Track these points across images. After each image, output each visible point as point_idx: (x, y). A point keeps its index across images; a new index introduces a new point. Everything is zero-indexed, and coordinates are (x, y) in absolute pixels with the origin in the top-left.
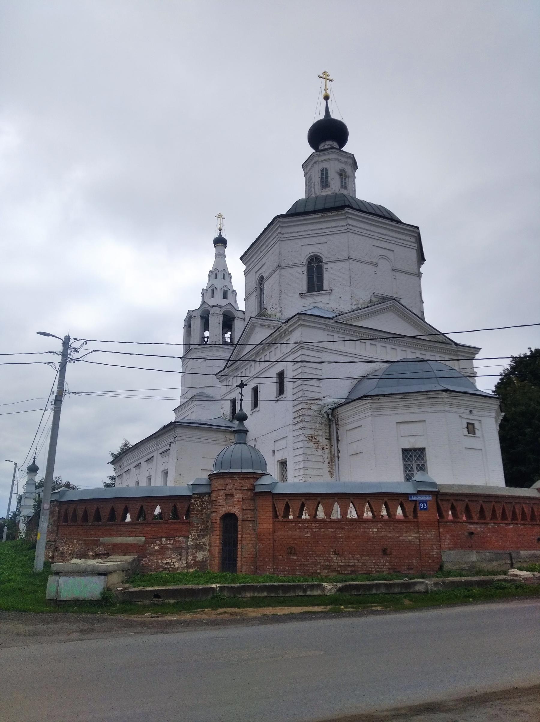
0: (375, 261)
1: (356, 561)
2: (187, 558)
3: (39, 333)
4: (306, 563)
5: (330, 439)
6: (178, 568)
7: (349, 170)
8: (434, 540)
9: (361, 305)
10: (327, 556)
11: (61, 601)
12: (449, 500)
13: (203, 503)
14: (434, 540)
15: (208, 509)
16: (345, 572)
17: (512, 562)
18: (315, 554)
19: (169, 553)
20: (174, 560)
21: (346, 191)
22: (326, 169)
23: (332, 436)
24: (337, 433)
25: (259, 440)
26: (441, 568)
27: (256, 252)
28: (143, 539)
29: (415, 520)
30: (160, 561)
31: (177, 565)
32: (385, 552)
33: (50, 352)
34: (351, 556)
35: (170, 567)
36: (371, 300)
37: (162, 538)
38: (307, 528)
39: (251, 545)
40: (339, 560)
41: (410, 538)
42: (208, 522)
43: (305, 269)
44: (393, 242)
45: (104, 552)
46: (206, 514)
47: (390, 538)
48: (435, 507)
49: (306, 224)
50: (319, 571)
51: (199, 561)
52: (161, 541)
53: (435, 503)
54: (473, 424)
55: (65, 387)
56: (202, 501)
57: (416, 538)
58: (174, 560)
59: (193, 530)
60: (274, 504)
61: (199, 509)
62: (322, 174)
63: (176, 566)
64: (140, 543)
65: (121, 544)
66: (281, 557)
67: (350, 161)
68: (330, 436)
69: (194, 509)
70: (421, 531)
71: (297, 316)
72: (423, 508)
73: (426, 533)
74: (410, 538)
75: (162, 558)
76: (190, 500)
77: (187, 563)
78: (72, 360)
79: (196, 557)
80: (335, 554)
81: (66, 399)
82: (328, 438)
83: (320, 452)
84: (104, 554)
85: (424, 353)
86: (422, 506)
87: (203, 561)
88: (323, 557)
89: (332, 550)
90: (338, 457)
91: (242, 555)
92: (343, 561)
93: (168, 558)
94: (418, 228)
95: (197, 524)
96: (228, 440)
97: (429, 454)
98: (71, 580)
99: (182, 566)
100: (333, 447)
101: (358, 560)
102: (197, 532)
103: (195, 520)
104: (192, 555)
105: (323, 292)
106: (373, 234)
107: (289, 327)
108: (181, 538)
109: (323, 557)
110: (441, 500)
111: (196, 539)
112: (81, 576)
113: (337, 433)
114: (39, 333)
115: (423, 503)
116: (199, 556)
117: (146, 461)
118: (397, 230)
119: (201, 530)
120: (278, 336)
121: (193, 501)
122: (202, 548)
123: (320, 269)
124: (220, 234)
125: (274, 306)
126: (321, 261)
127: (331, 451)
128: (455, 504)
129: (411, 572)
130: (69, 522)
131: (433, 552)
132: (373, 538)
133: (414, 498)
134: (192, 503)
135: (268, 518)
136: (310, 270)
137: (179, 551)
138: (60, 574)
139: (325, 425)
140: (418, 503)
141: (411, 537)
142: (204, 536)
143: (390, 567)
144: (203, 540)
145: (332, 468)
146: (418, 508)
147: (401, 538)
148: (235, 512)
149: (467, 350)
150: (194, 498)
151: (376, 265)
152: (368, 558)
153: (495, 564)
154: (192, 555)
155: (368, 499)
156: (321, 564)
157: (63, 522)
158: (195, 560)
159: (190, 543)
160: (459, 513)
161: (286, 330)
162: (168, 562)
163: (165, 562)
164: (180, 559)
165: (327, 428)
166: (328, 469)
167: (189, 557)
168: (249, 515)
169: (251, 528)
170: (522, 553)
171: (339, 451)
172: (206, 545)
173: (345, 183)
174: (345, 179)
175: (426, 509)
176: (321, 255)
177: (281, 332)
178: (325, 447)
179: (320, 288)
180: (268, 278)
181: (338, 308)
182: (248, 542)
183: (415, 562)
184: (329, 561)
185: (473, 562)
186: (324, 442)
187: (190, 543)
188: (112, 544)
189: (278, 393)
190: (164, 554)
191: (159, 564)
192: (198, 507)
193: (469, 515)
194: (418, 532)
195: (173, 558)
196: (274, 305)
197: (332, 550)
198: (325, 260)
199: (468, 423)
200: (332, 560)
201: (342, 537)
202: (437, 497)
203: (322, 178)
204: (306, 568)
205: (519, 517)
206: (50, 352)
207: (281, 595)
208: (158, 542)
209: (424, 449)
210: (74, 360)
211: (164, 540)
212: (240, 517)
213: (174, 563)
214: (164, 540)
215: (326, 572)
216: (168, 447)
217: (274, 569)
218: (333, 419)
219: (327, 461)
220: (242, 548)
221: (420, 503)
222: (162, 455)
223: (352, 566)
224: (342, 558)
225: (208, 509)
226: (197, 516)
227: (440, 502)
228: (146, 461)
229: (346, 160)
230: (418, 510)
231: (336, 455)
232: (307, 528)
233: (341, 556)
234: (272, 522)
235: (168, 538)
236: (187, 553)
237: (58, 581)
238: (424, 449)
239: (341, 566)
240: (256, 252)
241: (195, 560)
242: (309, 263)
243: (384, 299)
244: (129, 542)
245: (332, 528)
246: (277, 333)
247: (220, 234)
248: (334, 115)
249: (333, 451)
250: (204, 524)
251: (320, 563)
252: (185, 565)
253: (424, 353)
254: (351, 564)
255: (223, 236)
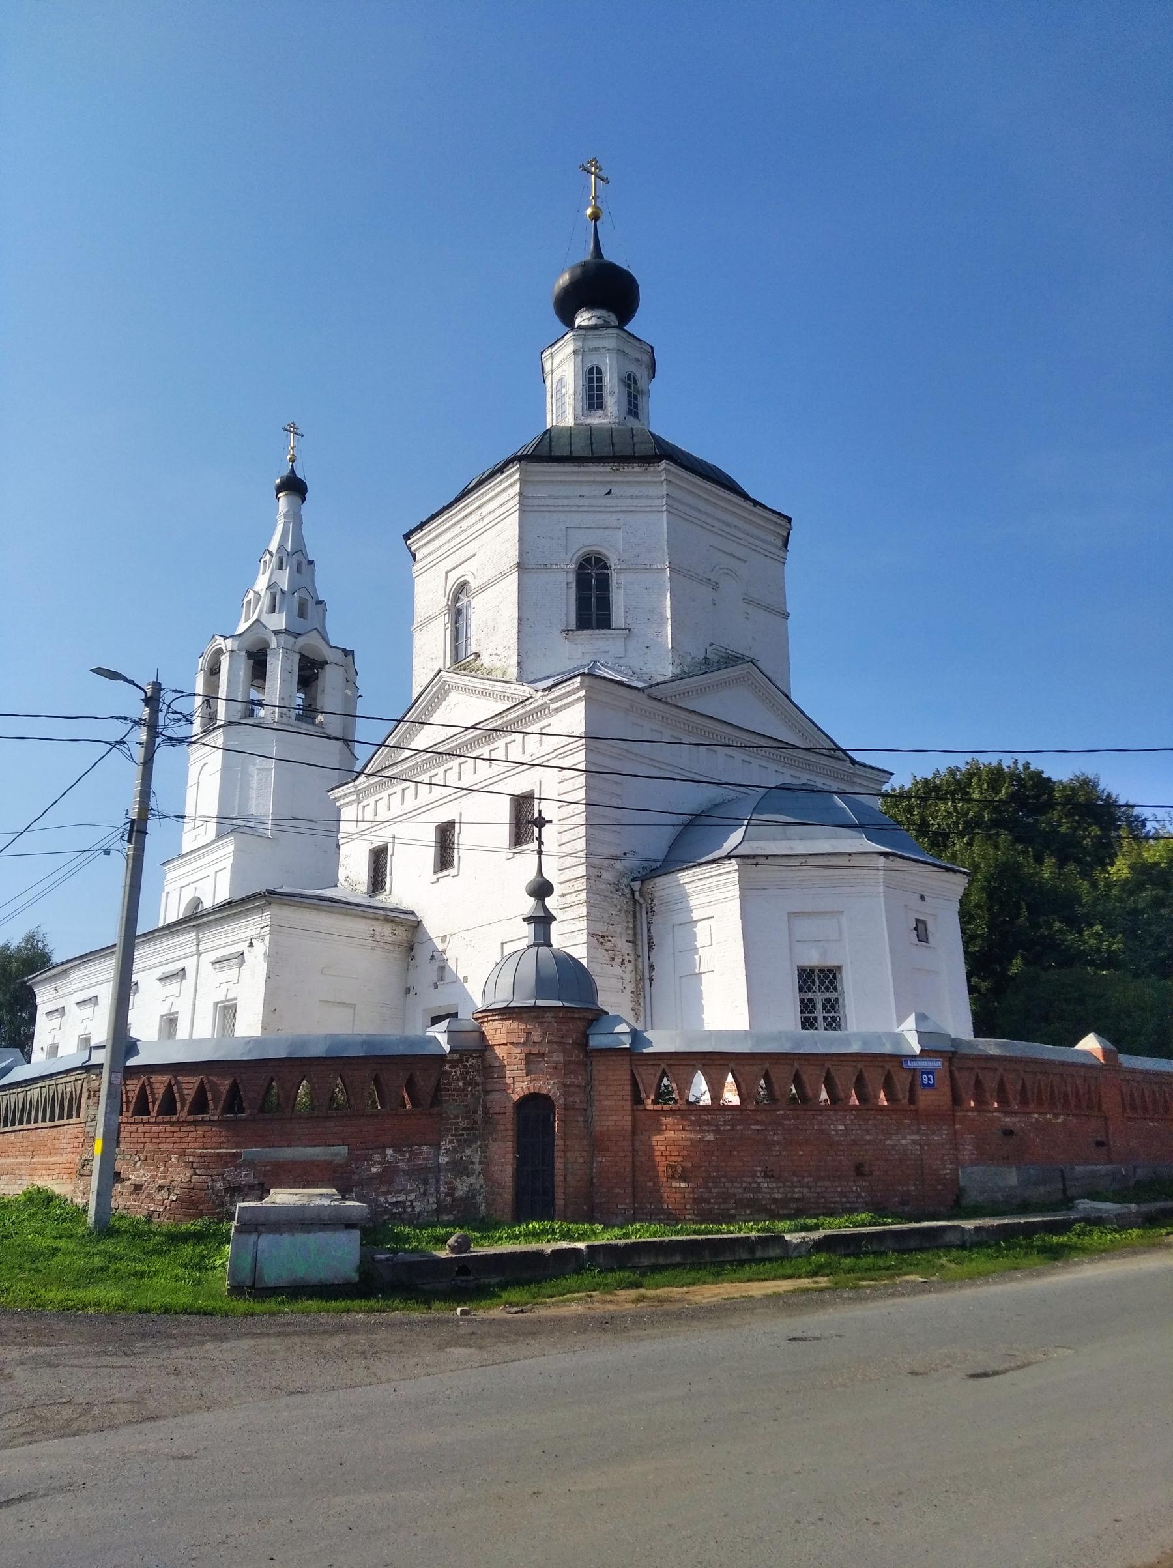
0: (713, 577)
1: (805, 1190)
2: (438, 1192)
3: (99, 671)
4: (706, 1196)
5: (633, 942)
6: (420, 1213)
7: (641, 374)
8: (947, 1147)
9: (689, 667)
10: (749, 1180)
11: (263, 1289)
12: (972, 1069)
13: (468, 1073)
14: (947, 1147)
15: (477, 1084)
16: (785, 1212)
17: (1064, 1185)
18: (725, 1176)
19: (400, 1181)
20: (412, 1196)
21: (636, 421)
22: (599, 371)
23: (639, 937)
24: (649, 930)
25: (455, 939)
26: (957, 1202)
27: (448, 529)
28: (344, 1150)
29: (912, 1107)
30: (382, 1199)
31: (418, 1207)
32: (859, 1171)
33: (119, 718)
34: (795, 1179)
35: (405, 1212)
36: (706, 658)
37: (385, 1147)
38: (708, 1123)
39: (581, 1160)
40: (772, 1188)
41: (903, 1142)
42: (475, 1112)
43: (572, 578)
44: (746, 543)
45: (252, 1180)
46: (472, 1095)
47: (869, 1142)
48: (948, 1083)
49: (576, 482)
50: (732, 1212)
51: (461, 1198)
52: (384, 1155)
53: (948, 1074)
54: (924, 923)
55: (153, 803)
56: (465, 1066)
57: (914, 1142)
58: (412, 1196)
59: (448, 1130)
60: (633, 1076)
61: (460, 1084)
62: (590, 380)
63: (417, 1210)
64: (338, 1160)
65: (294, 1163)
66: (650, 1184)
67: (646, 358)
68: (635, 935)
69: (449, 1084)
70: (924, 1128)
71: (579, 679)
72: (928, 1085)
73: (933, 1133)
74: (903, 1142)
75: (389, 1192)
76: (442, 1066)
77: (438, 1202)
78: (170, 739)
79: (454, 1189)
80: (766, 1176)
81: (152, 825)
82: (631, 939)
83: (617, 970)
84: (252, 1187)
85: (797, 774)
86: (925, 1078)
87: (467, 1198)
88: (741, 1183)
89: (759, 1169)
90: (651, 980)
91: (565, 1182)
92: (782, 1190)
93: (400, 1192)
94: (789, 520)
95: (456, 1117)
96: (378, 937)
97: (848, 980)
98: (286, 1239)
99: (429, 1208)
100: (640, 960)
101: (809, 1188)
102: (455, 1135)
103: (452, 1108)
104: (446, 1183)
105: (608, 631)
106: (709, 520)
107: (553, 700)
108: (425, 1148)
109: (741, 1183)
110: (959, 1069)
111: (455, 1150)
112: (309, 1232)
113: (649, 930)
114: (99, 671)
115: (927, 1074)
116: (460, 1187)
117: (160, 979)
118: (752, 518)
119: (463, 1129)
120: (520, 719)
121: (447, 1067)
122: (466, 1168)
123: (604, 583)
124: (292, 471)
125: (500, 650)
126: (606, 567)
127: (636, 966)
128: (981, 1077)
129: (906, 1209)
130: (153, 1114)
131: (945, 1169)
132: (839, 1143)
133: (912, 1064)
134: (446, 1072)
135: (622, 1103)
136: (582, 582)
137: (422, 1176)
138: (261, 1228)
139: (626, 911)
140: (918, 1073)
141: (907, 1140)
142: (469, 1143)
143: (868, 1199)
144: (468, 1152)
145: (638, 1003)
146: (918, 1083)
147: (888, 1142)
148: (550, 1091)
149: (870, 774)
150: (449, 1062)
151: (716, 586)
152: (827, 1183)
153: (1042, 1189)
154: (446, 1183)
155: (732, 1065)
156: (738, 1196)
157: (190, 1113)
158: (451, 1195)
159: (443, 1159)
160: (988, 1095)
161: (544, 707)
162: (399, 1199)
163: (394, 1200)
164: (425, 1194)
165: (631, 916)
166: (631, 1005)
167: (442, 1189)
168: (577, 1099)
169: (581, 1124)
170: (1079, 1169)
171: (652, 968)
172: (473, 1163)
173: (636, 406)
174: (636, 398)
175: (933, 1085)
176: (596, 548)
177: (528, 708)
178: (627, 958)
179: (604, 623)
180: (482, 589)
181: (644, 669)
182: (578, 1154)
183: (913, 1188)
184: (754, 1191)
185: (1011, 1188)
186: (624, 947)
187: (443, 1159)
188: (269, 1163)
189: (513, 840)
190: (391, 1182)
191: (380, 1206)
192: (458, 1080)
193: (1004, 1101)
194: (918, 1132)
195: (412, 1191)
196: (500, 648)
197: (759, 1169)
198: (613, 563)
199: (917, 921)
200: (759, 1189)
201: (779, 1143)
202: (951, 1064)
203: (591, 388)
204: (706, 1207)
205: (1073, 1102)
206: (119, 718)
207: (708, 1259)
208: (377, 1157)
209: (839, 968)
210: (174, 741)
211: (389, 1151)
212: (559, 1103)
213: (411, 1201)
214: (389, 1151)
215: (748, 1212)
216: (243, 947)
217: (634, 1209)
218: (641, 901)
219: (630, 987)
220: (565, 1169)
221: (923, 1073)
222: (217, 966)
223: (798, 1200)
224: (780, 1185)
225: (477, 1084)
226: (456, 1101)
227: (956, 1073)
228: (160, 979)
229: (638, 356)
230: (919, 1087)
231: (647, 975)
232: (708, 1123)
233: (778, 1179)
234: (629, 1112)
235: (397, 1149)
236: (438, 1181)
237: (256, 1244)
238: (839, 968)
239: (775, 1201)
240: (448, 529)
241: (451, 1195)
242: (581, 567)
243: (731, 660)
244: (315, 1158)
245: (757, 1123)
246: (520, 711)
247: (292, 471)
248: (611, 255)
249: (640, 967)
250: (467, 1118)
251: (735, 1194)
252: (435, 1206)
253: (797, 774)
254: (796, 1196)
255: (299, 475)
